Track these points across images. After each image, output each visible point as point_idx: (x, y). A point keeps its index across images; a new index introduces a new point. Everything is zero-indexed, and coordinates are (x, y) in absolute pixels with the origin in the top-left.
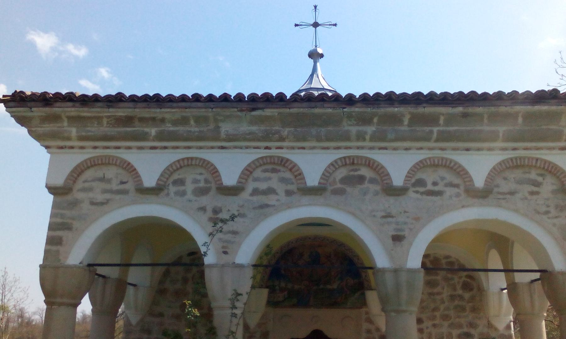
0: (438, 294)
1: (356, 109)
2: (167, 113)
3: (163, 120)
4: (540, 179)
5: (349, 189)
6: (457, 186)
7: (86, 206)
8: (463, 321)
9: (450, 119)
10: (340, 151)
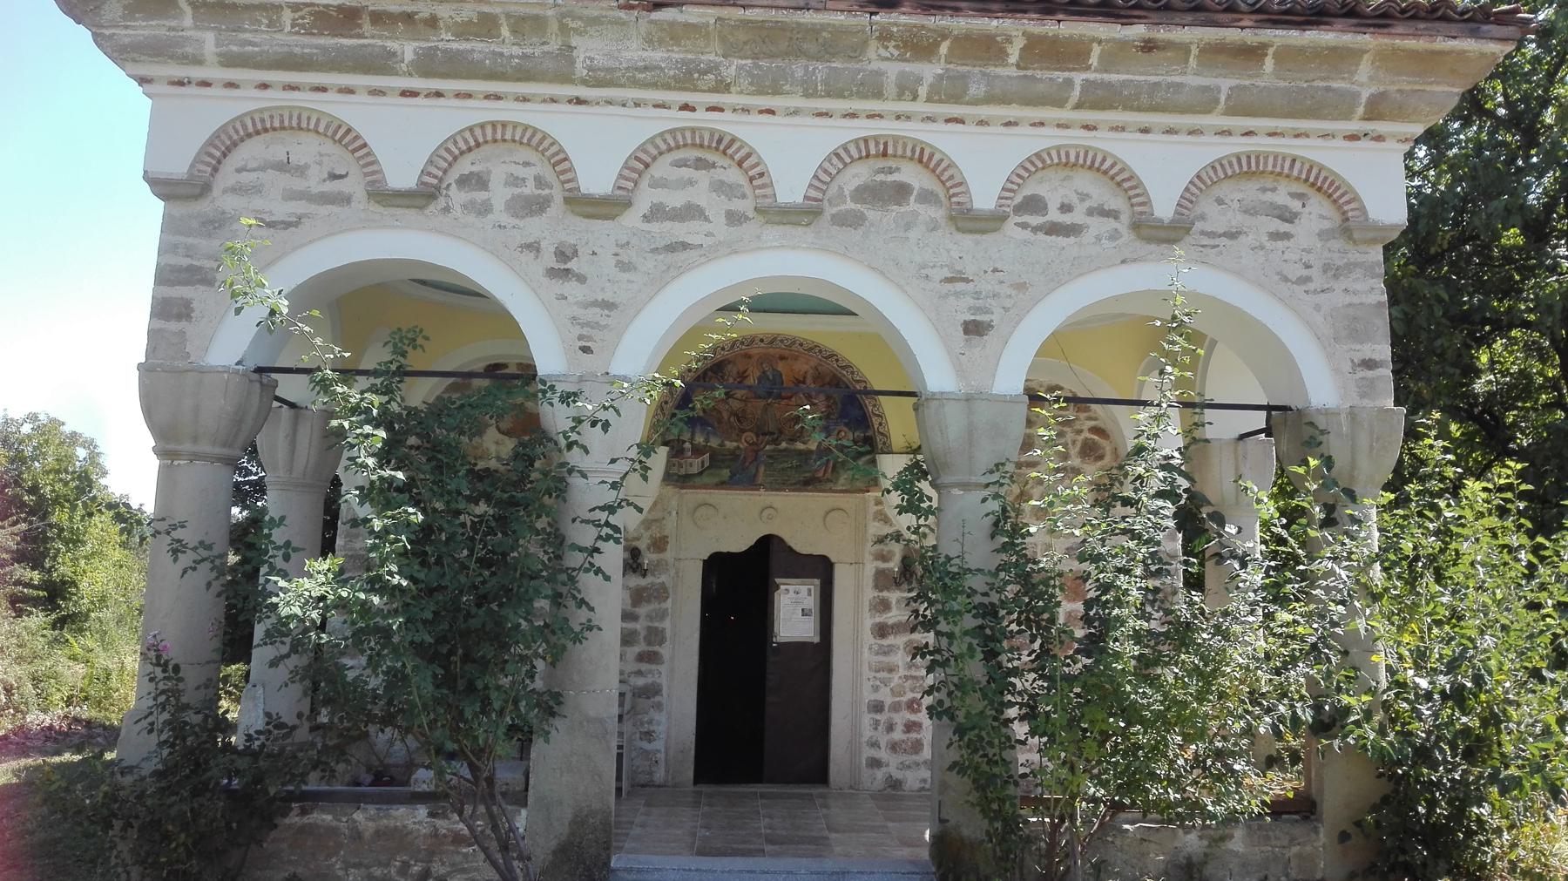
4: (1295, 205)
5: (872, 215)
6: (1113, 214)
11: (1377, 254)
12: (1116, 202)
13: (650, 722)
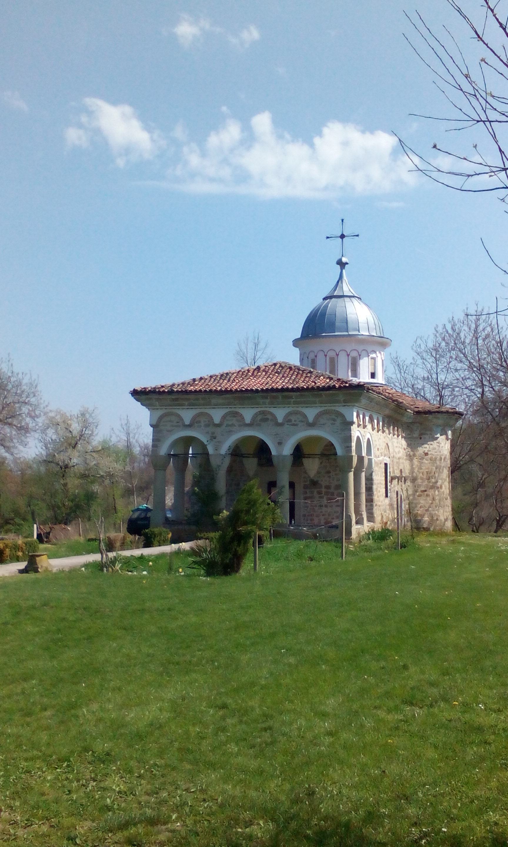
1: (260, 394)
2: (192, 396)
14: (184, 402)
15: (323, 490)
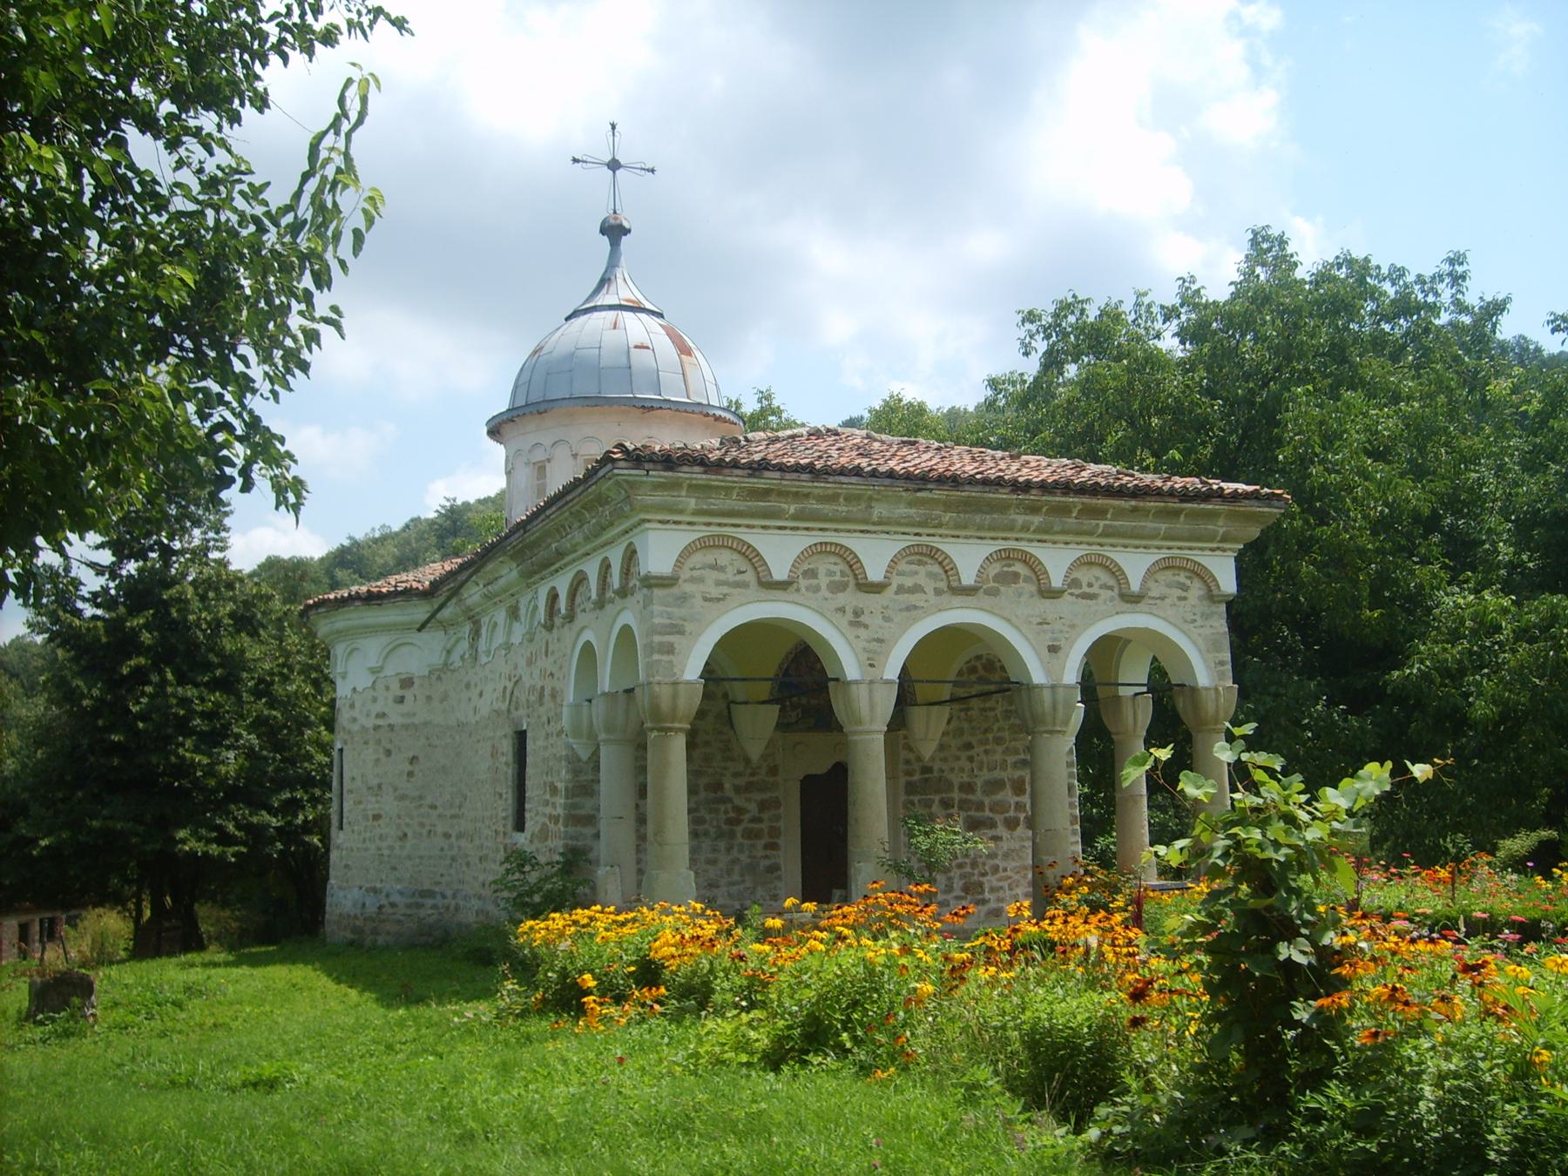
0: (992, 709)
3: (807, 496)
4: (1188, 582)
5: (1002, 589)
6: (1111, 588)
7: (698, 602)
8: (1019, 745)
9: (1119, 514)
10: (997, 542)
11: (1223, 608)
12: (1112, 582)
13: (775, 888)
14: (783, 505)
15: (956, 795)
